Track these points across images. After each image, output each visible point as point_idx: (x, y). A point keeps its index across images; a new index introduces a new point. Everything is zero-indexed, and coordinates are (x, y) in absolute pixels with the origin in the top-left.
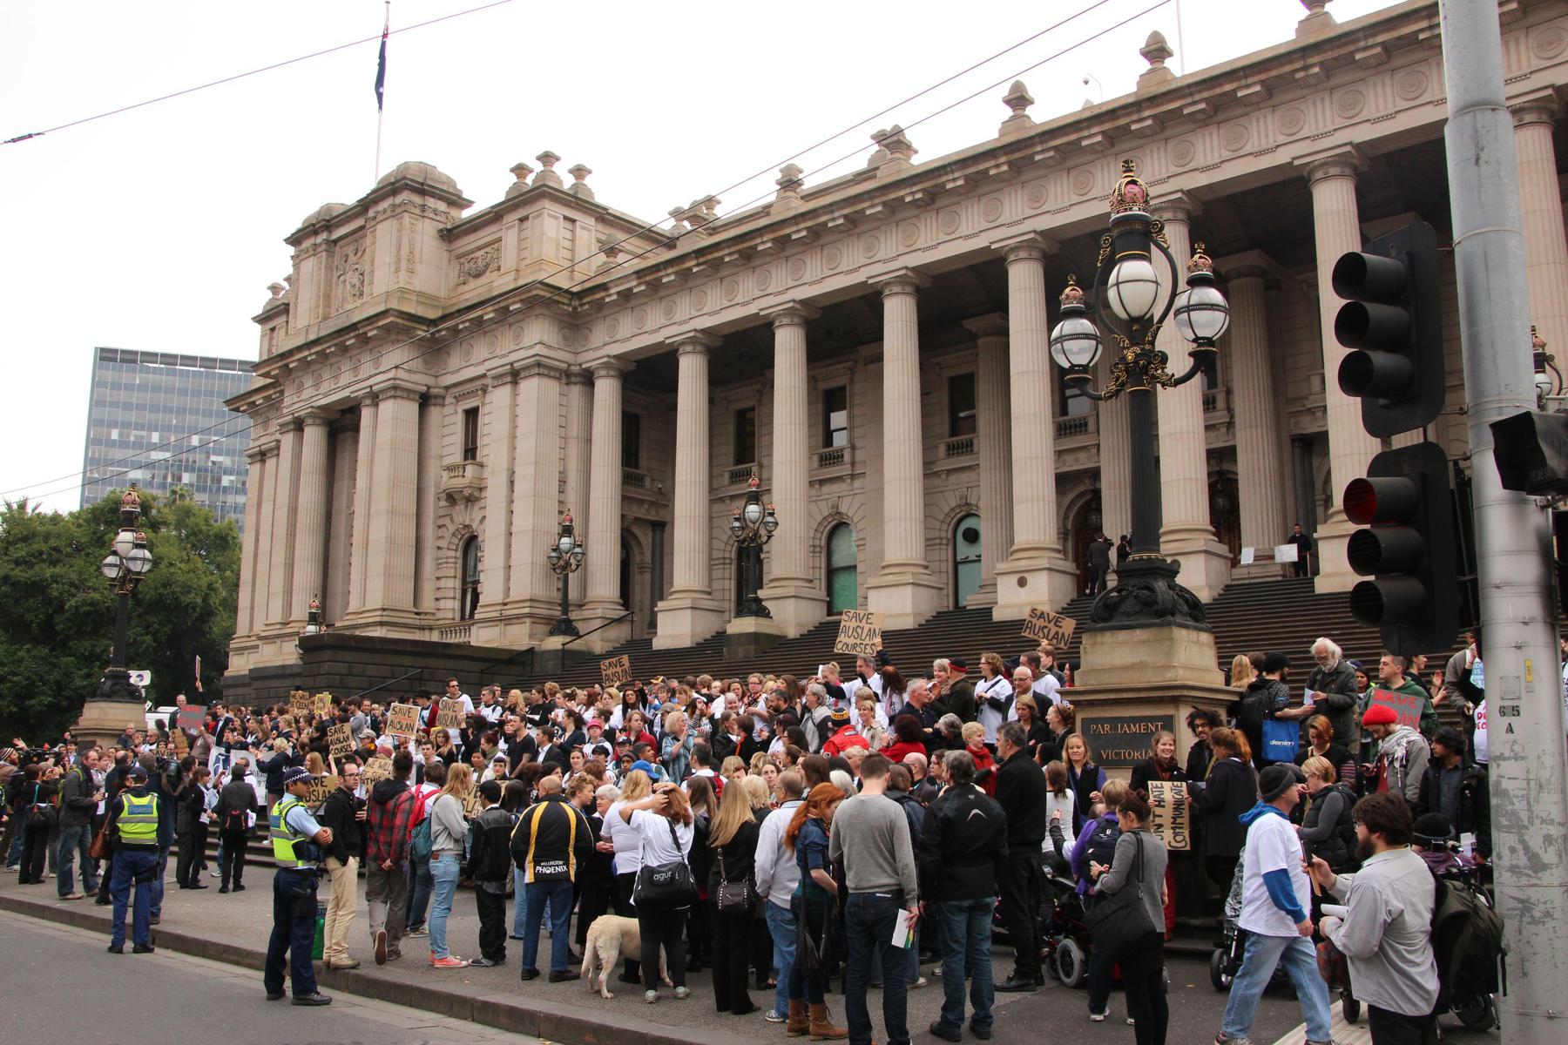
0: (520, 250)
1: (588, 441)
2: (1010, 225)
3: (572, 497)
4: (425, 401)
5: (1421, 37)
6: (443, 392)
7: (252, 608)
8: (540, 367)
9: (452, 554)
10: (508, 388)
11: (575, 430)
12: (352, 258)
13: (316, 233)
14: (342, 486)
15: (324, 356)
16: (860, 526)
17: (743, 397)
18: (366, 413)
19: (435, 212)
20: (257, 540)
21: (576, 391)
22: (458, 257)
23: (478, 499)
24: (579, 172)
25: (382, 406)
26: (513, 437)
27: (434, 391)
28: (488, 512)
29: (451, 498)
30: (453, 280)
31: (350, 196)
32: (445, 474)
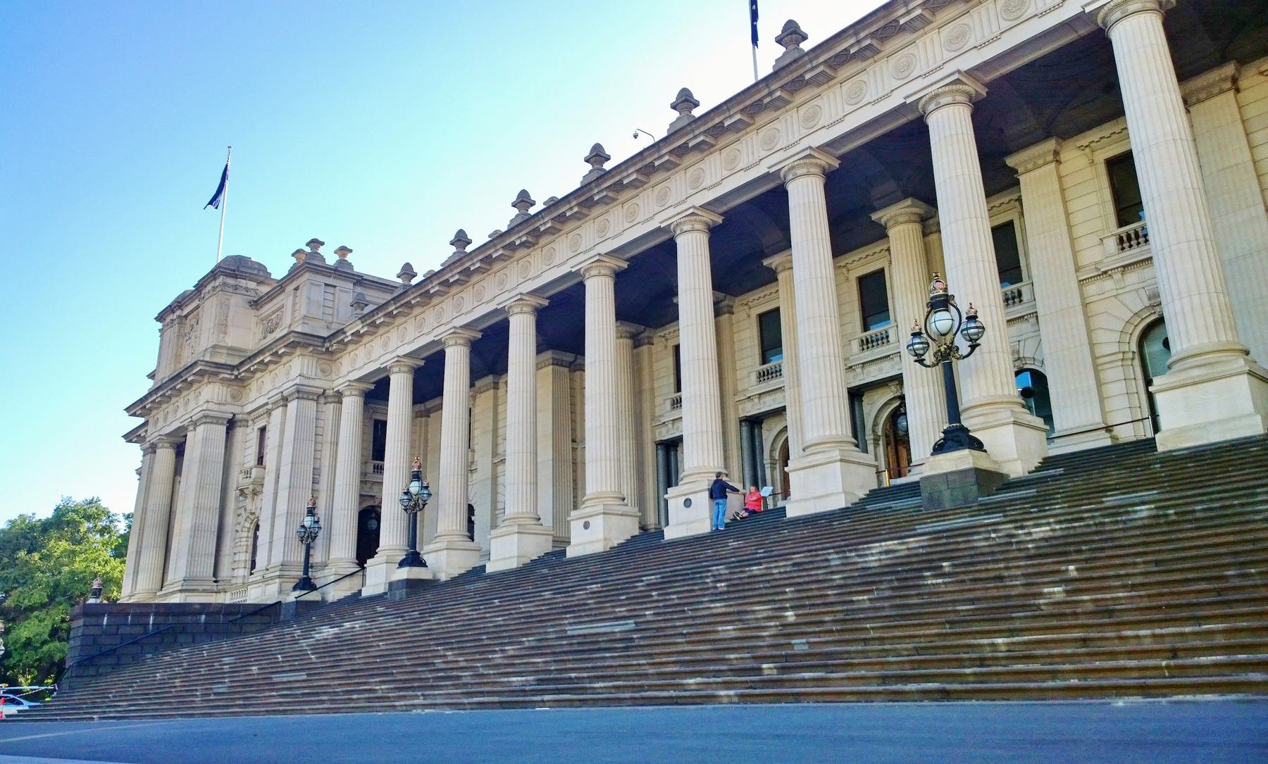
2: (585, 252)
5: (852, 51)
6: (246, 417)
8: (301, 393)
19: (247, 289)
24: (344, 250)
30: (259, 331)
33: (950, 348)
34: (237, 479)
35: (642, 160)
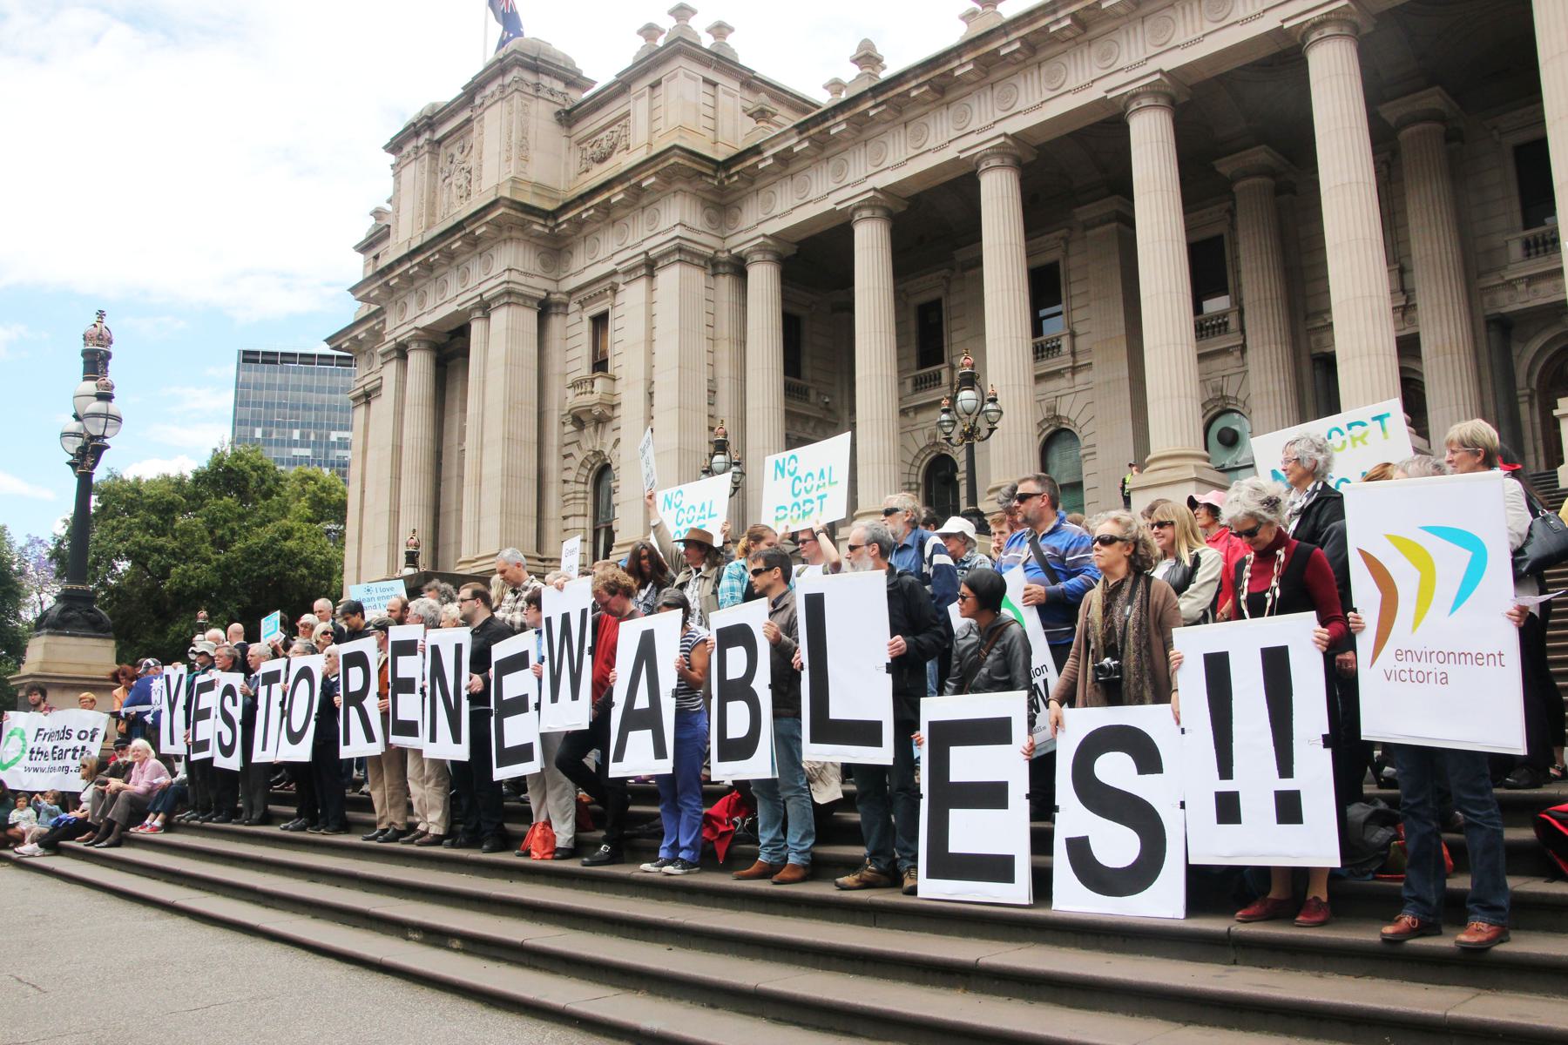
0: (652, 121)
1: (742, 343)
3: (725, 408)
4: (545, 309)
7: (359, 568)
8: (683, 253)
9: (581, 487)
10: (643, 283)
11: (725, 328)
12: (458, 157)
13: (417, 134)
14: (453, 422)
15: (428, 267)
16: (1085, 431)
17: (927, 288)
18: (476, 328)
20: (363, 492)
21: (725, 283)
22: (579, 143)
23: (610, 419)
24: (720, 30)
25: (495, 316)
26: (650, 341)
27: (555, 297)
28: (622, 434)
29: (578, 420)
30: (574, 168)
31: (449, 91)
32: (570, 393)
33: (972, 429)
34: (564, 399)
35: (1031, 23)
